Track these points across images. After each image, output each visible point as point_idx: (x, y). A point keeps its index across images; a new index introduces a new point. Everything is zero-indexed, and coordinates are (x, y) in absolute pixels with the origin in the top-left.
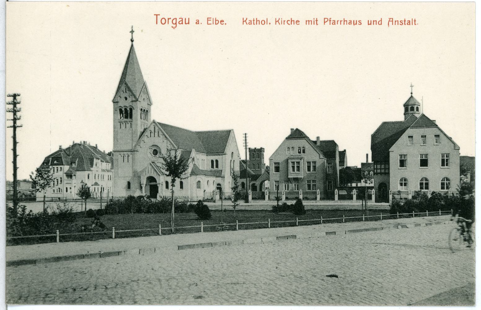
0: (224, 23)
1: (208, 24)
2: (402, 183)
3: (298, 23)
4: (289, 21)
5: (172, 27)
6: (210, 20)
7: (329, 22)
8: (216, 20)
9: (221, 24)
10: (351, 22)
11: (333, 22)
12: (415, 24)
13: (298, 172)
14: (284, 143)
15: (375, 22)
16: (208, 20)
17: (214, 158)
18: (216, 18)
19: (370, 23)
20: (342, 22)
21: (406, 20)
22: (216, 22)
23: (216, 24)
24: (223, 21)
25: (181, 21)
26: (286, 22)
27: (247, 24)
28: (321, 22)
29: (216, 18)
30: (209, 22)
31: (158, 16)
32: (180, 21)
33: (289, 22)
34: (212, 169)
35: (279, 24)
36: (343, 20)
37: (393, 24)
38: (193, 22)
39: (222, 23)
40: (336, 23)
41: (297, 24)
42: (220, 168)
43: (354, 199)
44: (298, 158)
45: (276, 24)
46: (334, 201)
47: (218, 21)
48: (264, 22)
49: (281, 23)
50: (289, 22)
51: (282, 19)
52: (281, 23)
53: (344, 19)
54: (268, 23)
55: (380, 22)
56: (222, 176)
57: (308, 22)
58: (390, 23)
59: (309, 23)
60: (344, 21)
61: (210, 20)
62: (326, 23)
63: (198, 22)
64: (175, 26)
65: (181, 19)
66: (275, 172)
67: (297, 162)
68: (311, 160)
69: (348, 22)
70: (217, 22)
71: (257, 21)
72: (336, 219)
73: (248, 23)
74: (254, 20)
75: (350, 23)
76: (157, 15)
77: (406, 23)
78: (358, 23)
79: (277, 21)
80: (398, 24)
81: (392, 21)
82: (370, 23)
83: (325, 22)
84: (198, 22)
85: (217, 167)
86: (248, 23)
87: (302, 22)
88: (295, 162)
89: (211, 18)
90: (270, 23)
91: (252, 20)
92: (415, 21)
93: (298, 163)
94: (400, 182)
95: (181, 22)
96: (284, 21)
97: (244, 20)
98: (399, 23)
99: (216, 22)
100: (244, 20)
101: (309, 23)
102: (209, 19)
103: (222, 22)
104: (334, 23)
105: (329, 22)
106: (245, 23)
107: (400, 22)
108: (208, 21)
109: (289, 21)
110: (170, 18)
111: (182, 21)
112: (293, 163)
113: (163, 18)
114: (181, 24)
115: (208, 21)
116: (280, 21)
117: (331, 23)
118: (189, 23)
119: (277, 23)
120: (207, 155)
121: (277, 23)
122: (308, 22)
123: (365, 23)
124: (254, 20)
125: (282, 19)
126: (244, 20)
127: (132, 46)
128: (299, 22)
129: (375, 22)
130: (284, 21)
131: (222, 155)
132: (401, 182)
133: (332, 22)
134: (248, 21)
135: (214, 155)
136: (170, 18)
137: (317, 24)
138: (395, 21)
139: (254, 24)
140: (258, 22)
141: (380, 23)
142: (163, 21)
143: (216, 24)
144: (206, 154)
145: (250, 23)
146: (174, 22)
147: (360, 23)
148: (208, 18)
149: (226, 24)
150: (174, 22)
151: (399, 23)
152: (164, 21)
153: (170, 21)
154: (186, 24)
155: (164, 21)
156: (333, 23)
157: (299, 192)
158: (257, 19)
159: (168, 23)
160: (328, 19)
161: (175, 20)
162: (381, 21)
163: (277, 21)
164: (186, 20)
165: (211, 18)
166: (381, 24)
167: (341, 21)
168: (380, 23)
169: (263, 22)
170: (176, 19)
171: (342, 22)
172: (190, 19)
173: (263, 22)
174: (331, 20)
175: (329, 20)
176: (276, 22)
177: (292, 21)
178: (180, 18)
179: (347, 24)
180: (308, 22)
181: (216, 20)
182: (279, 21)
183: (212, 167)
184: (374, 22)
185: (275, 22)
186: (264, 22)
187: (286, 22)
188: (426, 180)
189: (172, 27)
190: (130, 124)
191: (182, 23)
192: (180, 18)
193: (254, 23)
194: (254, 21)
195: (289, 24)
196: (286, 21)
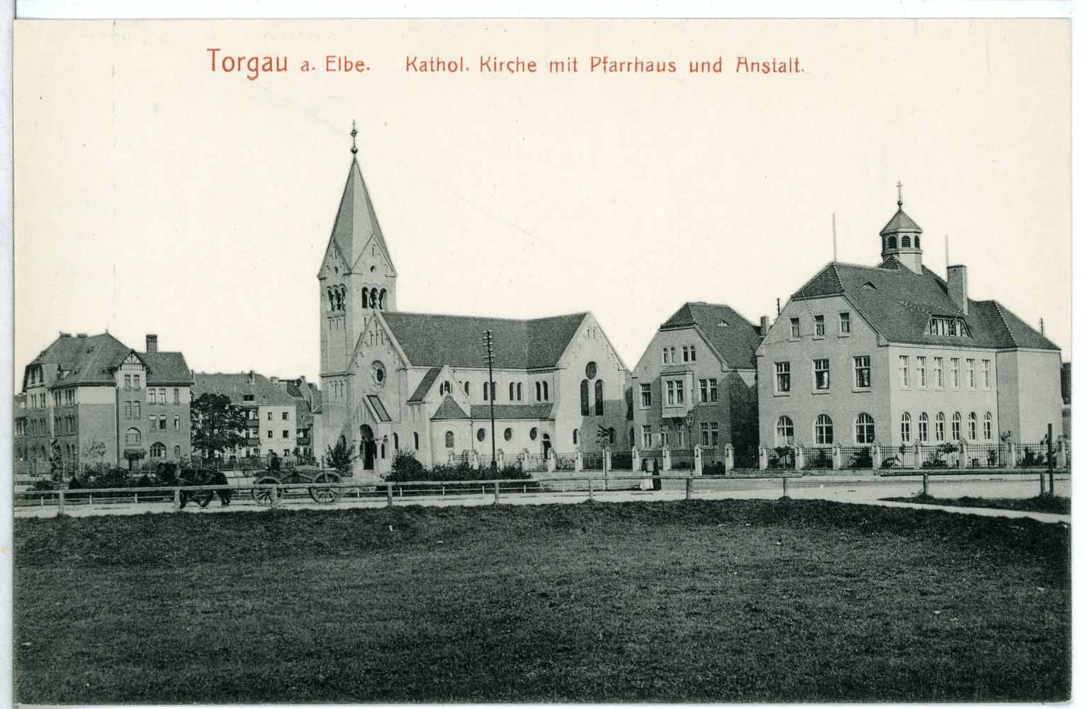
0: (365, 67)
1: (328, 70)
2: (863, 427)
3: (532, 68)
4: (513, 62)
5: (248, 77)
6: (334, 62)
7: (602, 65)
8: (347, 60)
9: (531, 71)
10: (270, 63)
11: (648, 65)
12: (797, 71)
13: (679, 405)
14: (657, 334)
15: (706, 66)
16: (328, 62)
17: (541, 377)
18: (346, 58)
19: (694, 68)
20: (631, 65)
21: (778, 62)
22: (347, 66)
23: (346, 70)
24: (363, 64)
25: (594, 64)
26: (504, 66)
27: (416, 70)
28: (584, 65)
29: (438, 58)
30: (331, 66)
31: (216, 52)
32: (266, 64)
33: (513, 66)
34: (539, 402)
35: (490, 70)
36: (634, 63)
37: (747, 71)
38: (294, 65)
39: (360, 68)
40: (700, 68)
41: (357, 69)
42: (551, 400)
43: (634, 468)
44: (678, 373)
45: (408, 70)
46: (830, 472)
47: (715, 71)
48: (454, 67)
49: (492, 68)
50: (513, 66)
51: (495, 58)
52: (492, 67)
53: (636, 58)
54: (464, 69)
55: (718, 65)
56: (551, 417)
57: (554, 66)
58: (742, 67)
59: (557, 68)
60: (637, 64)
61: (334, 62)
62: (597, 67)
63: (306, 67)
64: (254, 74)
65: (268, 60)
66: (643, 405)
67: (677, 382)
68: (706, 376)
69: (645, 66)
70: (349, 66)
71: (438, 63)
72: (399, 511)
73: (418, 68)
74: (432, 62)
75: (650, 68)
76: (214, 50)
77: (777, 69)
78: (667, 67)
79: (483, 63)
80: (758, 71)
81: (746, 63)
82: (694, 68)
83: (593, 66)
84: (306, 67)
85: (546, 397)
86: (418, 69)
87: (682, 66)
88: (674, 382)
89: (335, 57)
90: (468, 69)
91: (771, 61)
92: (797, 63)
93: (680, 383)
94: (859, 424)
95: (267, 67)
96: (501, 64)
97: (410, 62)
98: (761, 67)
99: (347, 66)
100: (410, 61)
101: (557, 68)
102: (330, 59)
103: (532, 66)
104: (614, 68)
105: (602, 65)
106: (411, 67)
107: (670, 64)
108: (329, 63)
109: (513, 62)
110: (244, 58)
111: (268, 67)
112: (670, 383)
113: (226, 58)
114: (267, 70)
115: (329, 63)
116: (491, 65)
117: (608, 69)
118: (285, 69)
119: (485, 67)
120: (528, 373)
121: (485, 67)
122: (554, 66)
123: (682, 66)
124: (432, 62)
125: (495, 58)
126: (410, 61)
127: (355, 161)
128: (535, 65)
129: (706, 66)
130: (501, 64)
131: (552, 371)
132: (861, 424)
133: (608, 66)
134: (418, 65)
135: (541, 372)
136: (244, 58)
137: (575, 70)
138: (753, 64)
139: (432, 70)
140: (441, 65)
141: (717, 67)
142: (228, 64)
143: (346, 70)
144: (526, 370)
145: (424, 67)
146: (253, 65)
147: (672, 69)
148: (328, 57)
149: (368, 69)
150: (253, 65)
151: (761, 67)
152: (231, 64)
153: (244, 64)
154: (278, 70)
155: (231, 64)
156: (611, 67)
157: (661, 451)
158: (346, 58)
159: (239, 69)
160: (600, 60)
161: (254, 61)
162: (720, 63)
163: (483, 63)
164: (280, 62)
165: (335, 57)
166: (720, 70)
167: (629, 64)
168: (718, 67)
169: (453, 67)
170: (257, 59)
171: (632, 67)
172: (287, 59)
173: (453, 67)
174: (607, 60)
175: (602, 60)
176: (408, 65)
177: (518, 64)
178: (265, 58)
179: (642, 70)
180: (555, 66)
181: (346, 62)
182: (488, 64)
183: (539, 398)
184: (283, 67)
185: (737, 63)
186: (454, 67)
187: (504, 66)
188: (870, 419)
189: (248, 77)
190: (342, 322)
191: (271, 69)
192: (265, 58)
193: (575, 69)
194: (433, 64)
195: (512, 71)
196: (247, 60)
